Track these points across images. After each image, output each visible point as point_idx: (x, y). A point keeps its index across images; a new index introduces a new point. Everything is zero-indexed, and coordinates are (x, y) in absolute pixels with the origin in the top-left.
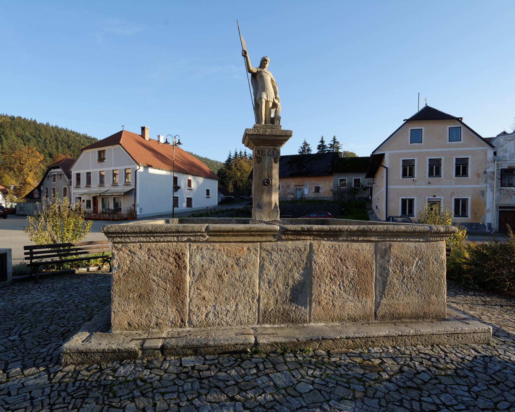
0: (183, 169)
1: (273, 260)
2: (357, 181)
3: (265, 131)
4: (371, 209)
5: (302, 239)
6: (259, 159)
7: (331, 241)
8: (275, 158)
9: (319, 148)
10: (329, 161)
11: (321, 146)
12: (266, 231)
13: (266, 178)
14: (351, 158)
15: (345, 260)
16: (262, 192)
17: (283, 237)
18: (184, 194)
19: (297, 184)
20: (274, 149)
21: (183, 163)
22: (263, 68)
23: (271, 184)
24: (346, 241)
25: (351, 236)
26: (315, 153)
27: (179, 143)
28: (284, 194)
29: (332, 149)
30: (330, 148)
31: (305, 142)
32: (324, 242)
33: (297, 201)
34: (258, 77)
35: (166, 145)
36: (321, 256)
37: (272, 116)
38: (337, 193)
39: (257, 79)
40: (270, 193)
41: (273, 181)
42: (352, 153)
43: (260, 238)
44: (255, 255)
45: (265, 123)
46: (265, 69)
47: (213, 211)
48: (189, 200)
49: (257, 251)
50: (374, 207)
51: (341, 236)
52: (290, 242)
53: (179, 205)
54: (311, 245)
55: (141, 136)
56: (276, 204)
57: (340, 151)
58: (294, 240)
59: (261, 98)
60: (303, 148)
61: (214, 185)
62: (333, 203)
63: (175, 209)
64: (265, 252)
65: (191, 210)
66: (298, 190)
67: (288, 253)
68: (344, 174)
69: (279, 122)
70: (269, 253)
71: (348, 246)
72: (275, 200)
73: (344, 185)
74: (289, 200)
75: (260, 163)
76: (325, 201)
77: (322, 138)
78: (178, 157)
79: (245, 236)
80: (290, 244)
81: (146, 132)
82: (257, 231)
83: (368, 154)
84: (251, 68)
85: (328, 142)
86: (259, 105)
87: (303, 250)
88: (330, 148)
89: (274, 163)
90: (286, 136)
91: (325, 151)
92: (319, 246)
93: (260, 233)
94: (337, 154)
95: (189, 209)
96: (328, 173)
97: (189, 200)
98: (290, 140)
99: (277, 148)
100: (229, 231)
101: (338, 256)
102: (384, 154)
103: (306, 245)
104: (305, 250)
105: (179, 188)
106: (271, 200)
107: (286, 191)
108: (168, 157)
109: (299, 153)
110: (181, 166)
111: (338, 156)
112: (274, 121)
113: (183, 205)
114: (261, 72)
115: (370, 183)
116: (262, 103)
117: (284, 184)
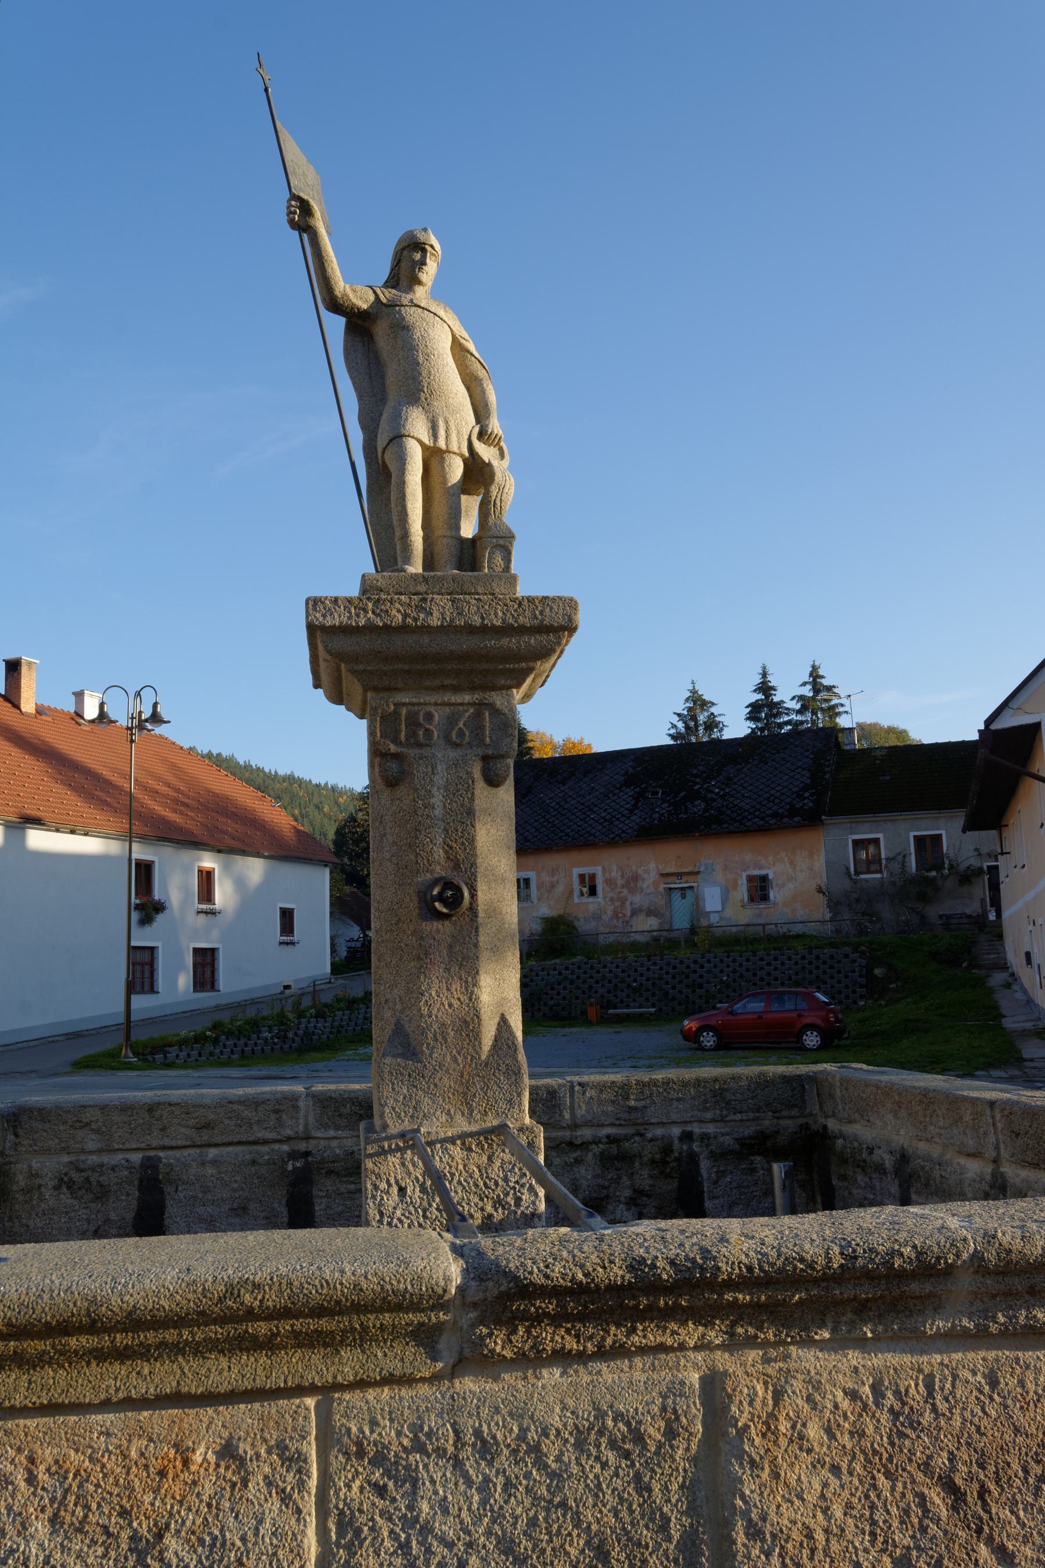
0: (179, 829)
1: (426, 1530)
2: (928, 846)
3: (420, 608)
4: (1004, 967)
5: (643, 1350)
6: (393, 766)
7: (862, 1344)
8: (485, 759)
9: (752, 716)
10: (796, 768)
11: (765, 706)
12: (359, 1308)
13: (439, 871)
14: (895, 748)
15: (983, 1492)
16: (422, 957)
17: (497, 1344)
18: (179, 935)
19: (672, 870)
20: (480, 706)
21: (178, 804)
22: (410, 289)
23: (473, 909)
24: (979, 1338)
25: (1009, 1298)
26: (741, 735)
27: (156, 718)
28: (616, 915)
29: (808, 716)
30: (799, 712)
31: (694, 692)
32: (808, 1359)
33: (673, 944)
34: (381, 330)
35: (100, 728)
36: (798, 1472)
37: (468, 529)
38: (846, 899)
39: (377, 350)
40: (465, 963)
41: (481, 887)
42: (891, 730)
43: (316, 1358)
44: (286, 1498)
45: (429, 563)
46: (420, 294)
47: (306, 1002)
48: (205, 963)
49: (295, 1461)
50: (1015, 960)
51: (934, 1304)
52: (552, 1375)
53: (161, 984)
54: (714, 1386)
55: (6, 698)
56: (503, 1022)
57: (844, 722)
58: (582, 1357)
59: (398, 438)
60: (690, 718)
61: (312, 889)
62: (833, 945)
63: (140, 1002)
64: (363, 1467)
65: (212, 1003)
66: (676, 896)
67: (541, 1464)
68: (869, 817)
69: (508, 560)
70: (392, 1472)
71: (994, 1383)
72: (502, 1002)
73: (873, 864)
74: (639, 938)
75: (402, 790)
76: (798, 936)
77: (764, 675)
78: (158, 779)
79: (199, 1350)
80: (555, 1395)
81: (24, 682)
82: (285, 1313)
83: (966, 729)
84: (341, 285)
85: (789, 690)
86: (388, 474)
87: (654, 1432)
88: (799, 712)
89: (480, 785)
90: (545, 631)
91: (781, 726)
92: (778, 1396)
93: (313, 1324)
94: (832, 735)
95: (206, 999)
96: (805, 815)
97: (205, 963)
98: (574, 648)
99: (498, 699)
100: (64, 1328)
101: (926, 1467)
102: (1037, 726)
103: (677, 1389)
104: (671, 1433)
105: (159, 907)
106: (472, 999)
107: (623, 901)
108: (106, 773)
109: (672, 737)
110: (158, 809)
111: (837, 744)
112: (474, 557)
113: (177, 983)
114: (393, 305)
115: (984, 850)
116: (402, 460)
117: (615, 873)
